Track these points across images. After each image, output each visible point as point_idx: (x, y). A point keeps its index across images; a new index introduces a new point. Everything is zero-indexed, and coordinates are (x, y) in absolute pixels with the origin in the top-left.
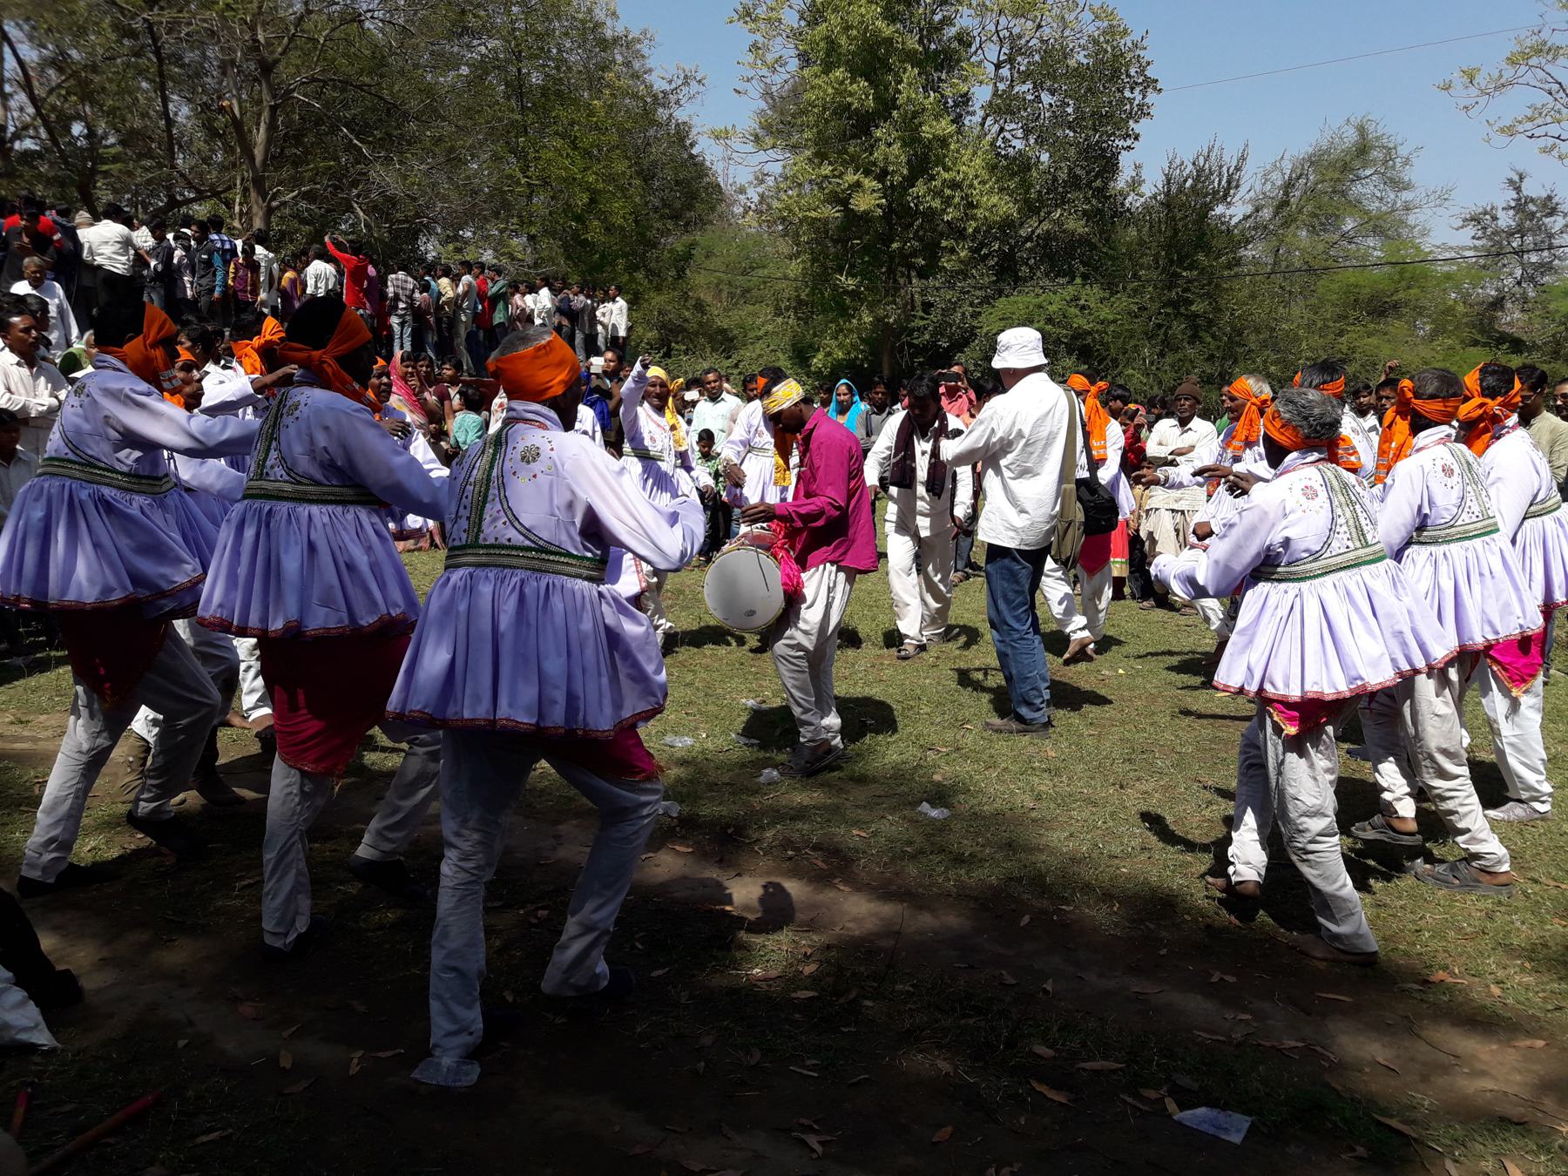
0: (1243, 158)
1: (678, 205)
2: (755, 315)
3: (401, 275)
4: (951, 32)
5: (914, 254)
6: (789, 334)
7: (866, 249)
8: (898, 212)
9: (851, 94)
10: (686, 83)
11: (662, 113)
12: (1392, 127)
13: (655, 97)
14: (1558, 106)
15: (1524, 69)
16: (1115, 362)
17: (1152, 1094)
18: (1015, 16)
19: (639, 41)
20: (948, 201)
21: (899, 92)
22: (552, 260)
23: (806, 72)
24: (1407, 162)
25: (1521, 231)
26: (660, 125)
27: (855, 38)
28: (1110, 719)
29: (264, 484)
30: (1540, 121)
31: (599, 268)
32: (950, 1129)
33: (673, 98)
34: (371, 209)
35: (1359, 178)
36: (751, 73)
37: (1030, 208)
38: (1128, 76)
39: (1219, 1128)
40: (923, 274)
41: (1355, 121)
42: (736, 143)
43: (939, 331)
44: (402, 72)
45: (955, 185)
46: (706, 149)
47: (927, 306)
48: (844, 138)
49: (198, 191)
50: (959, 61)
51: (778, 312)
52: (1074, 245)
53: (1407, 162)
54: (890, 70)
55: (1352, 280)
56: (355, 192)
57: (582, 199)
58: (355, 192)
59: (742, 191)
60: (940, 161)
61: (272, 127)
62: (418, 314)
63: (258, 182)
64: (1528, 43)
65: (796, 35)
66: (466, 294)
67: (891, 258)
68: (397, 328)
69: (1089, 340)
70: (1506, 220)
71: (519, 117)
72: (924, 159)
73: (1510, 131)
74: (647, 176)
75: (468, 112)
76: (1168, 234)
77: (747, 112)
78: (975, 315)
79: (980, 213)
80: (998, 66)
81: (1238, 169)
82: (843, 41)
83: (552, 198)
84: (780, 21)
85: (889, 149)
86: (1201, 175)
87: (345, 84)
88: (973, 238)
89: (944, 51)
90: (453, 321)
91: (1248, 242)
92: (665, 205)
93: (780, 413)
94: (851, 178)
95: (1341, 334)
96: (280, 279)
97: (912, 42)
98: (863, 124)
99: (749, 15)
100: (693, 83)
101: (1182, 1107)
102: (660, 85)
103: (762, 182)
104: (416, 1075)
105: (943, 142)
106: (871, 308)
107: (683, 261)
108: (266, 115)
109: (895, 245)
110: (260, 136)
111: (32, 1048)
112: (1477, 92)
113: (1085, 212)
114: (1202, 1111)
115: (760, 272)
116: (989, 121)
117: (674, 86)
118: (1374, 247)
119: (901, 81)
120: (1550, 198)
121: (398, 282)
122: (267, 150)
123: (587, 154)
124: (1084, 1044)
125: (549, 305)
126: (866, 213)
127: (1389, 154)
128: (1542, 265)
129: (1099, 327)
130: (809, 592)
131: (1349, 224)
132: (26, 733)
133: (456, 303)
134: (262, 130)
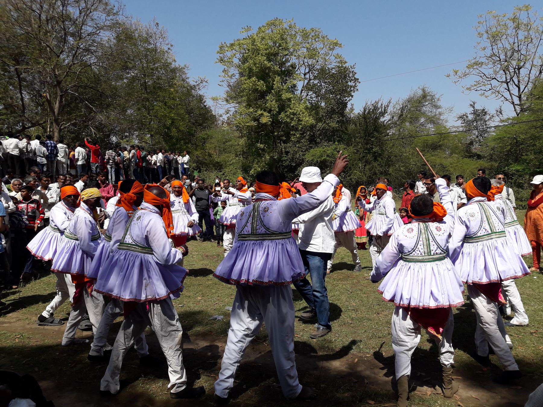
0: (390, 102)
2: (228, 157)
5: (282, 136)
6: (241, 163)
7: (266, 135)
8: (276, 123)
9: (258, 86)
16: (350, 168)
18: (310, 58)
20: (292, 119)
23: (242, 78)
25: (476, 120)
27: (258, 67)
28: (370, 291)
30: (479, 86)
31: (174, 144)
33: (197, 87)
34: (96, 128)
37: (319, 120)
38: (350, 77)
40: (285, 142)
41: (421, 87)
42: (220, 102)
43: (292, 160)
44: (105, 82)
45: (294, 114)
46: (209, 103)
47: (287, 153)
48: (256, 100)
49: (32, 123)
50: (292, 74)
51: (237, 156)
52: (334, 131)
53: (438, 100)
54: (270, 77)
56: (90, 122)
57: (169, 122)
58: (90, 122)
59: (221, 116)
60: (289, 106)
61: (61, 102)
62: (116, 164)
63: (56, 121)
65: (239, 66)
66: (133, 157)
67: (274, 138)
68: (109, 169)
70: (471, 117)
71: (146, 95)
74: (189, 112)
75: (129, 94)
77: (222, 92)
78: (304, 155)
79: (303, 123)
80: (305, 75)
82: (254, 68)
83: (159, 122)
84: (232, 62)
86: (376, 108)
87: (86, 87)
88: (301, 130)
89: (287, 71)
90: (129, 166)
94: (260, 112)
96: (69, 154)
97: (277, 68)
98: (262, 95)
99: (222, 60)
100: (204, 82)
102: (192, 83)
103: (228, 113)
105: (289, 100)
106: (269, 154)
107: (204, 140)
108: (59, 98)
110: (57, 106)
119: (274, 81)
120: (484, 110)
121: (109, 153)
122: (59, 110)
123: (170, 107)
125: (161, 158)
126: (265, 123)
127: (433, 97)
131: (422, 120)
132: (6, 320)
133: (129, 160)
134: (57, 103)
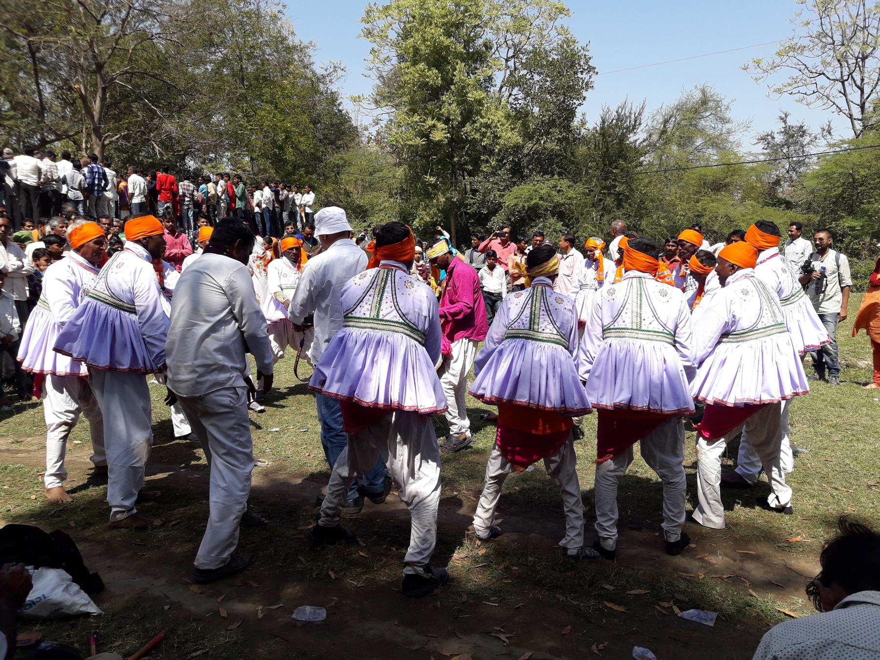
0: (643, 108)
1: (333, 137)
2: (378, 197)
3: (186, 182)
4: (480, 42)
5: (466, 163)
7: (439, 162)
8: (456, 141)
10: (335, 71)
11: (321, 87)
12: (718, 90)
13: (318, 79)
14: (805, 77)
15: (785, 58)
16: (577, 219)
17: (666, 605)
18: (516, 33)
19: (307, 47)
21: (454, 76)
22: (265, 170)
24: (727, 108)
25: (787, 144)
26: (322, 93)
27: (429, 46)
29: (531, 332)
32: (569, 627)
34: (162, 143)
35: (703, 117)
36: (372, 65)
37: (528, 136)
38: (579, 64)
39: (702, 619)
40: (471, 174)
41: (700, 87)
42: (364, 103)
45: (487, 126)
46: (347, 106)
47: (474, 192)
48: (425, 101)
49: (57, 135)
51: (391, 196)
52: (552, 157)
53: (727, 108)
54: (449, 63)
55: (703, 172)
57: (281, 137)
60: (478, 113)
61: (103, 99)
63: (96, 131)
64: (787, 45)
65: (396, 45)
67: (453, 166)
69: (563, 208)
72: (469, 113)
73: (779, 91)
74: (315, 122)
76: (605, 150)
77: (369, 86)
78: (502, 196)
79: (501, 141)
80: (507, 60)
81: (640, 114)
82: (423, 48)
85: (450, 107)
86: (620, 118)
88: (499, 154)
91: (645, 154)
92: (325, 138)
93: (436, 258)
94: (430, 122)
95: (698, 202)
97: (460, 48)
98: (435, 93)
99: (370, 33)
100: (339, 70)
101: (682, 609)
102: (319, 72)
103: (377, 124)
104: (294, 616)
105: (480, 102)
106: (444, 193)
107: (338, 169)
109: (456, 159)
110: (96, 106)
111: (88, 615)
112: (762, 71)
113: (559, 139)
114: (692, 611)
115: (381, 174)
116: (504, 89)
117: (328, 72)
118: (712, 155)
119: (455, 70)
120: (801, 127)
122: (101, 112)
124: (628, 582)
127: (718, 103)
128: (799, 162)
129: (568, 201)
130: (454, 353)
131: (699, 142)
132: (22, 448)
